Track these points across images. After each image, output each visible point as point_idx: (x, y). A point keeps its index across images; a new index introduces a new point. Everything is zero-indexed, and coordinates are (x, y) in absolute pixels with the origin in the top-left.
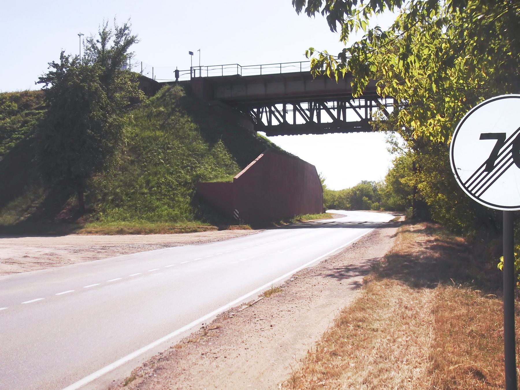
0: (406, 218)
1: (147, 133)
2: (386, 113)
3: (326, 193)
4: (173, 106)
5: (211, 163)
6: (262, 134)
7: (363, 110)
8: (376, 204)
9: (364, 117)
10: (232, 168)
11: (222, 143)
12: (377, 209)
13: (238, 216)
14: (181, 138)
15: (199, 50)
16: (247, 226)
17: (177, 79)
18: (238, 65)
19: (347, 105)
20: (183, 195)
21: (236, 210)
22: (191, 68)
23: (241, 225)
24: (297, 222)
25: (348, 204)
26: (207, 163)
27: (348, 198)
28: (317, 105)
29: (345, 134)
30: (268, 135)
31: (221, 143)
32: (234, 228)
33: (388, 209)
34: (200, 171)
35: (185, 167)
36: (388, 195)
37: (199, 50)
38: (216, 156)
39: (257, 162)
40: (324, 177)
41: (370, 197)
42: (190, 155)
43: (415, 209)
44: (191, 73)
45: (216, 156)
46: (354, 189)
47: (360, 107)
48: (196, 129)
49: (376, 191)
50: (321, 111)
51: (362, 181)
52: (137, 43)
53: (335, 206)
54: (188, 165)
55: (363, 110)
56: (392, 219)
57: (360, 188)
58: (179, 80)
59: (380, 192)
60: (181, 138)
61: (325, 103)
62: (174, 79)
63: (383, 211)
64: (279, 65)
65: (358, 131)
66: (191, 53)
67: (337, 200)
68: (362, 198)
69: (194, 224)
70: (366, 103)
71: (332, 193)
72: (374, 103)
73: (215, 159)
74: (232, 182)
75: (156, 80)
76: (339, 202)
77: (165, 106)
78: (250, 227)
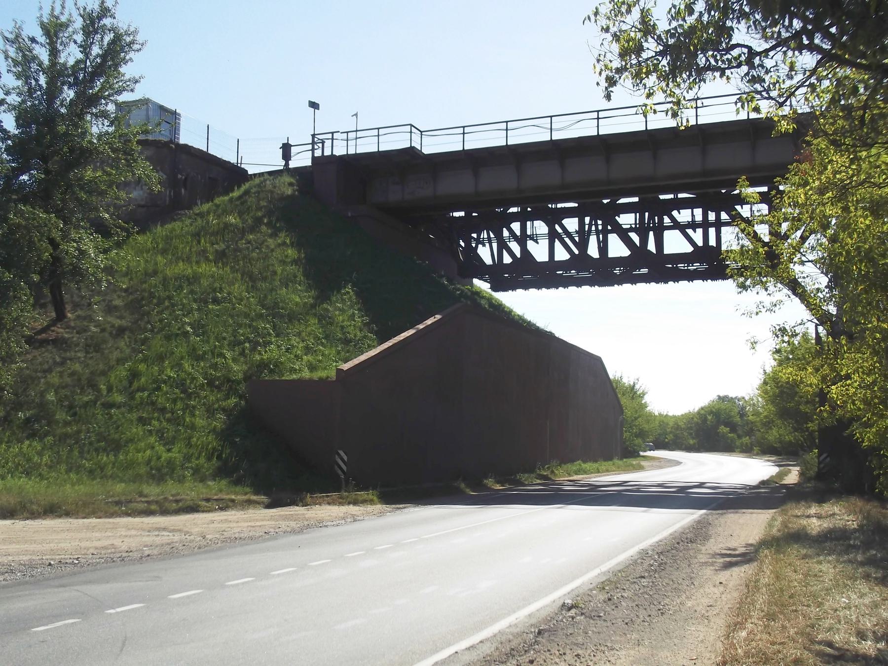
0: (802, 474)
1: (181, 268)
2: (756, 237)
3: (645, 418)
4: (260, 214)
5: (310, 334)
6: (482, 285)
7: (700, 231)
8: (746, 440)
9: (700, 243)
10: (360, 348)
11: (353, 291)
12: (747, 451)
13: (344, 468)
14: (252, 278)
15: (356, 115)
16: (370, 494)
17: (287, 164)
18: (412, 126)
19: (667, 220)
20: (210, 412)
21: (341, 453)
22: (313, 136)
23: (346, 491)
24: (539, 481)
25: (693, 438)
26: (299, 334)
27: (691, 428)
28: (600, 222)
29: (661, 286)
30: (495, 288)
31: (348, 293)
32: (321, 500)
33: (766, 450)
34: (272, 352)
35: (240, 343)
36: (768, 424)
37: (356, 115)
38: (325, 320)
39: (419, 332)
40: (643, 388)
41: (733, 428)
42: (260, 316)
43: (824, 455)
44: (313, 150)
45: (325, 320)
46: (703, 412)
47: (693, 225)
48: (295, 262)
49: (745, 415)
50: (610, 236)
51: (719, 396)
52: (138, 50)
53: (668, 443)
54: (248, 338)
55: (700, 231)
56: (765, 479)
57: (714, 410)
58: (293, 164)
59: (751, 418)
60: (252, 278)
61: (617, 218)
62: (278, 163)
63: (757, 454)
64: (504, 126)
65: (691, 276)
66: (314, 105)
67: (671, 432)
68: (718, 428)
69: (215, 488)
70: (705, 215)
71: (663, 420)
72: (724, 216)
73: (322, 327)
74: (334, 378)
75: (243, 166)
76: (676, 436)
77: (240, 214)
78: (375, 498)
